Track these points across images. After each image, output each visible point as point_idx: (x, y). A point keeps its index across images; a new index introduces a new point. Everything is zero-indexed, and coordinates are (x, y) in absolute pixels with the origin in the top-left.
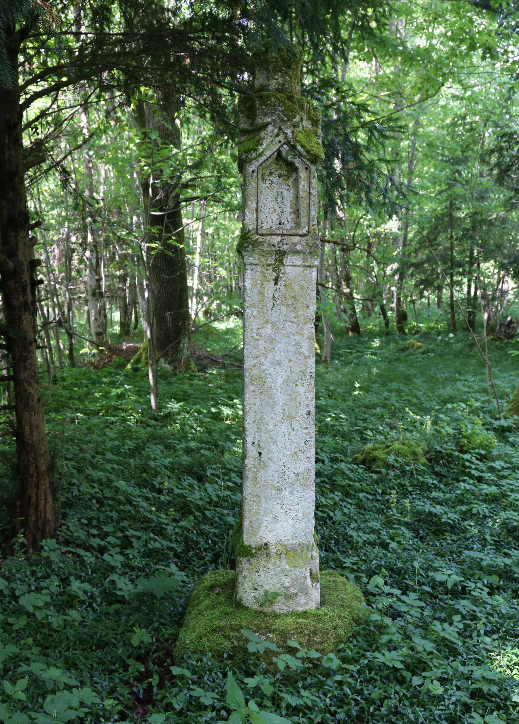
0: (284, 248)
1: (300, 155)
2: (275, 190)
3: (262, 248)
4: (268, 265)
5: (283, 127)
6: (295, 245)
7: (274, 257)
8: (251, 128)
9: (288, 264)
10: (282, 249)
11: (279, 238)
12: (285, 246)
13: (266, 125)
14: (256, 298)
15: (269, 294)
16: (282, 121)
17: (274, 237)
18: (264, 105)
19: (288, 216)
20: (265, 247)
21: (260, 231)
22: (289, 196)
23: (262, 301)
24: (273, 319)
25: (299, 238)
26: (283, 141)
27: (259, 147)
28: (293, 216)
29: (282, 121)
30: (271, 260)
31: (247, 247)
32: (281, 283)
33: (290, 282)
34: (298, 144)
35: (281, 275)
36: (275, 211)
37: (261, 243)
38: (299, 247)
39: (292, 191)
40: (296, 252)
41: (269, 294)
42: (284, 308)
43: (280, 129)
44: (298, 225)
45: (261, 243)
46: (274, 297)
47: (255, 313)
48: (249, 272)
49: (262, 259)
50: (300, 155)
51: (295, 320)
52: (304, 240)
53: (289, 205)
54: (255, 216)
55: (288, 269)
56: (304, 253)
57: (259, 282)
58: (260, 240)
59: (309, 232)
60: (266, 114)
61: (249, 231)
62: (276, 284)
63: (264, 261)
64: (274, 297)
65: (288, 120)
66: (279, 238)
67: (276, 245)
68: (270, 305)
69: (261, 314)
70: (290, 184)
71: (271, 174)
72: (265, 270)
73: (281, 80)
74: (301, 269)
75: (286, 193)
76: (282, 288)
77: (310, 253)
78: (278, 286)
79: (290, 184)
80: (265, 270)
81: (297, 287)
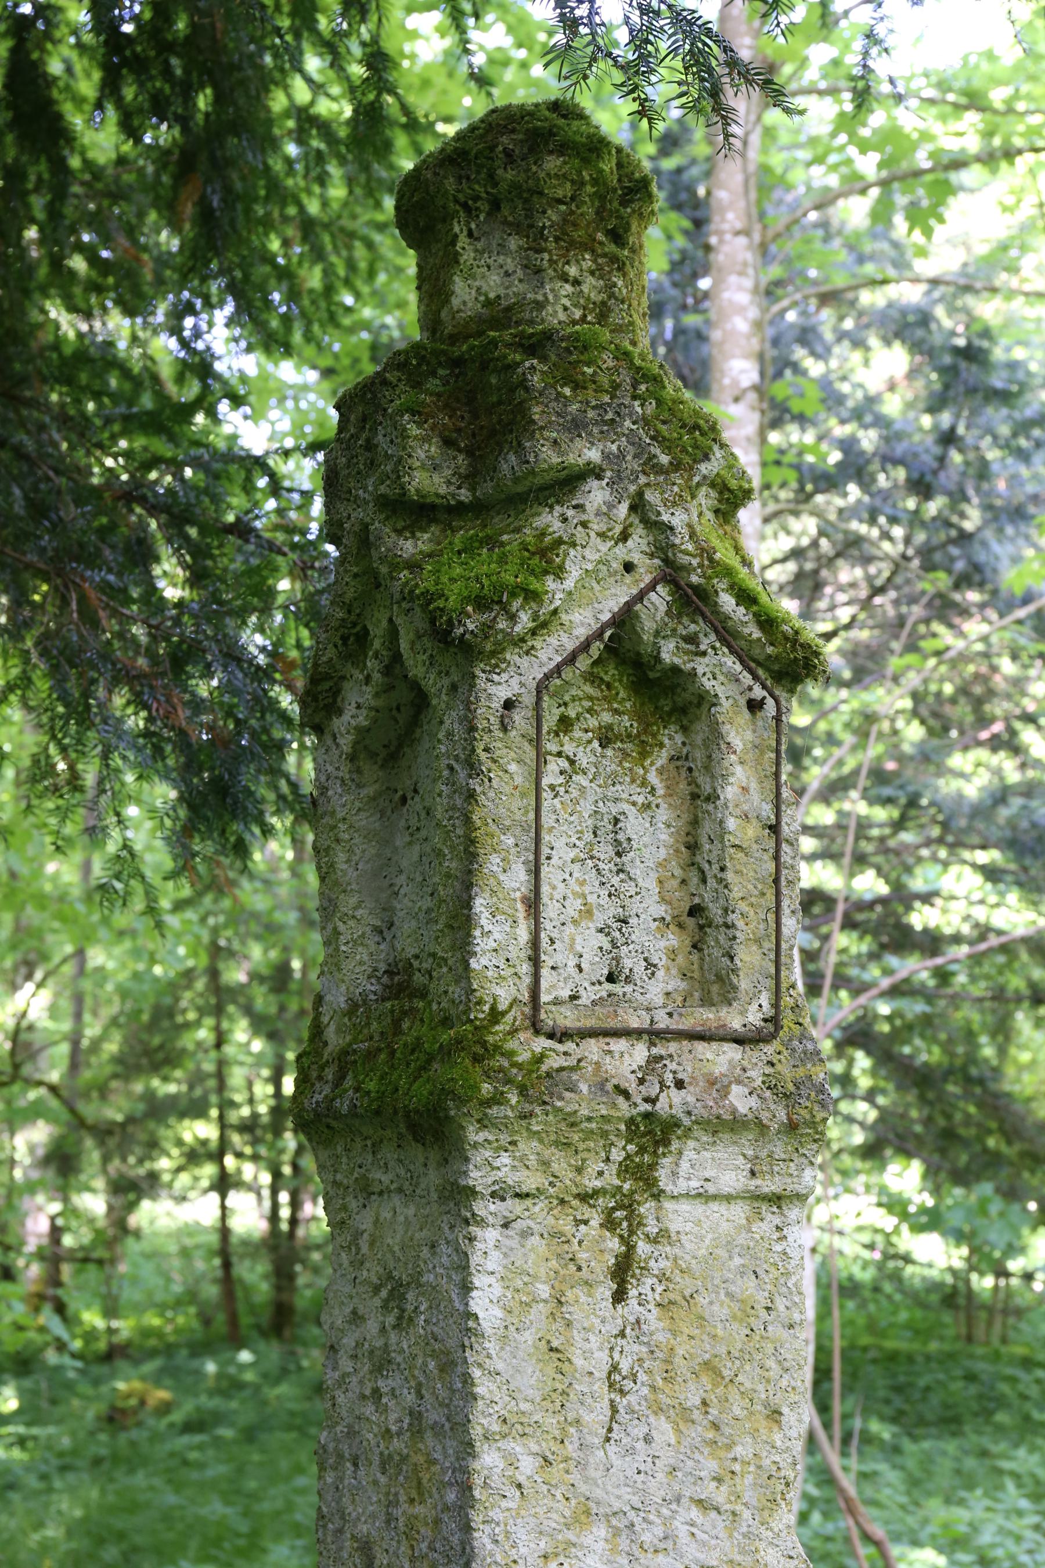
0: (672, 1102)
1: (727, 634)
2: (586, 807)
3: (568, 1103)
4: (585, 1197)
5: (652, 497)
6: (719, 1086)
7: (617, 1155)
8: (464, 495)
9: (682, 1186)
10: (662, 1107)
11: (640, 1053)
12: (676, 1096)
13: (568, 483)
14: (532, 1379)
15: (590, 1355)
16: (651, 466)
17: (619, 1045)
18: (568, 380)
19: (653, 941)
20: (582, 1101)
21: (548, 1018)
22: (652, 837)
23: (559, 1397)
24: (616, 1495)
25: (731, 1052)
26: (647, 568)
27: (550, 583)
28: (673, 939)
29: (651, 466)
30: (601, 1172)
31: (498, 1099)
32: (644, 1287)
33: (687, 1285)
34: (721, 585)
35: (642, 1248)
36: (587, 912)
37: (558, 1081)
38: (740, 1100)
39: (663, 814)
40: (726, 1126)
41: (590, 1355)
42: (664, 1430)
43: (638, 506)
44: (714, 984)
45: (558, 1081)
46: (615, 1368)
47: (528, 1465)
48: (489, 1236)
49: (561, 1163)
50: (727, 634)
51: (720, 1496)
52: (753, 1063)
53: (650, 883)
54: (523, 934)
55: (679, 1216)
56: (762, 1128)
57: (544, 1290)
58: (554, 1062)
59: (774, 1020)
60: (576, 427)
61: (496, 1016)
62: (619, 1296)
63: (568, 1176)
64: (615, 1368)
65: (676, 466)
66: (640, 1053)
67: (632, 1087)
68: (595, 1417)
69: (556, 1472)
70: (653, 778)
71: (565, 724)
72: (566, 1226)
73: (590, 286)
74: (739, 1211)
75: (634, 825)
76: (653, 1319)
77: (792, 1127)
78: (632, 1308)
79: (653, 778)
80: (566, 1226)
81: (720, 1310)
